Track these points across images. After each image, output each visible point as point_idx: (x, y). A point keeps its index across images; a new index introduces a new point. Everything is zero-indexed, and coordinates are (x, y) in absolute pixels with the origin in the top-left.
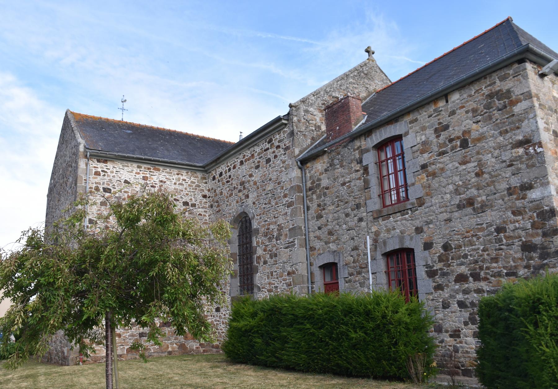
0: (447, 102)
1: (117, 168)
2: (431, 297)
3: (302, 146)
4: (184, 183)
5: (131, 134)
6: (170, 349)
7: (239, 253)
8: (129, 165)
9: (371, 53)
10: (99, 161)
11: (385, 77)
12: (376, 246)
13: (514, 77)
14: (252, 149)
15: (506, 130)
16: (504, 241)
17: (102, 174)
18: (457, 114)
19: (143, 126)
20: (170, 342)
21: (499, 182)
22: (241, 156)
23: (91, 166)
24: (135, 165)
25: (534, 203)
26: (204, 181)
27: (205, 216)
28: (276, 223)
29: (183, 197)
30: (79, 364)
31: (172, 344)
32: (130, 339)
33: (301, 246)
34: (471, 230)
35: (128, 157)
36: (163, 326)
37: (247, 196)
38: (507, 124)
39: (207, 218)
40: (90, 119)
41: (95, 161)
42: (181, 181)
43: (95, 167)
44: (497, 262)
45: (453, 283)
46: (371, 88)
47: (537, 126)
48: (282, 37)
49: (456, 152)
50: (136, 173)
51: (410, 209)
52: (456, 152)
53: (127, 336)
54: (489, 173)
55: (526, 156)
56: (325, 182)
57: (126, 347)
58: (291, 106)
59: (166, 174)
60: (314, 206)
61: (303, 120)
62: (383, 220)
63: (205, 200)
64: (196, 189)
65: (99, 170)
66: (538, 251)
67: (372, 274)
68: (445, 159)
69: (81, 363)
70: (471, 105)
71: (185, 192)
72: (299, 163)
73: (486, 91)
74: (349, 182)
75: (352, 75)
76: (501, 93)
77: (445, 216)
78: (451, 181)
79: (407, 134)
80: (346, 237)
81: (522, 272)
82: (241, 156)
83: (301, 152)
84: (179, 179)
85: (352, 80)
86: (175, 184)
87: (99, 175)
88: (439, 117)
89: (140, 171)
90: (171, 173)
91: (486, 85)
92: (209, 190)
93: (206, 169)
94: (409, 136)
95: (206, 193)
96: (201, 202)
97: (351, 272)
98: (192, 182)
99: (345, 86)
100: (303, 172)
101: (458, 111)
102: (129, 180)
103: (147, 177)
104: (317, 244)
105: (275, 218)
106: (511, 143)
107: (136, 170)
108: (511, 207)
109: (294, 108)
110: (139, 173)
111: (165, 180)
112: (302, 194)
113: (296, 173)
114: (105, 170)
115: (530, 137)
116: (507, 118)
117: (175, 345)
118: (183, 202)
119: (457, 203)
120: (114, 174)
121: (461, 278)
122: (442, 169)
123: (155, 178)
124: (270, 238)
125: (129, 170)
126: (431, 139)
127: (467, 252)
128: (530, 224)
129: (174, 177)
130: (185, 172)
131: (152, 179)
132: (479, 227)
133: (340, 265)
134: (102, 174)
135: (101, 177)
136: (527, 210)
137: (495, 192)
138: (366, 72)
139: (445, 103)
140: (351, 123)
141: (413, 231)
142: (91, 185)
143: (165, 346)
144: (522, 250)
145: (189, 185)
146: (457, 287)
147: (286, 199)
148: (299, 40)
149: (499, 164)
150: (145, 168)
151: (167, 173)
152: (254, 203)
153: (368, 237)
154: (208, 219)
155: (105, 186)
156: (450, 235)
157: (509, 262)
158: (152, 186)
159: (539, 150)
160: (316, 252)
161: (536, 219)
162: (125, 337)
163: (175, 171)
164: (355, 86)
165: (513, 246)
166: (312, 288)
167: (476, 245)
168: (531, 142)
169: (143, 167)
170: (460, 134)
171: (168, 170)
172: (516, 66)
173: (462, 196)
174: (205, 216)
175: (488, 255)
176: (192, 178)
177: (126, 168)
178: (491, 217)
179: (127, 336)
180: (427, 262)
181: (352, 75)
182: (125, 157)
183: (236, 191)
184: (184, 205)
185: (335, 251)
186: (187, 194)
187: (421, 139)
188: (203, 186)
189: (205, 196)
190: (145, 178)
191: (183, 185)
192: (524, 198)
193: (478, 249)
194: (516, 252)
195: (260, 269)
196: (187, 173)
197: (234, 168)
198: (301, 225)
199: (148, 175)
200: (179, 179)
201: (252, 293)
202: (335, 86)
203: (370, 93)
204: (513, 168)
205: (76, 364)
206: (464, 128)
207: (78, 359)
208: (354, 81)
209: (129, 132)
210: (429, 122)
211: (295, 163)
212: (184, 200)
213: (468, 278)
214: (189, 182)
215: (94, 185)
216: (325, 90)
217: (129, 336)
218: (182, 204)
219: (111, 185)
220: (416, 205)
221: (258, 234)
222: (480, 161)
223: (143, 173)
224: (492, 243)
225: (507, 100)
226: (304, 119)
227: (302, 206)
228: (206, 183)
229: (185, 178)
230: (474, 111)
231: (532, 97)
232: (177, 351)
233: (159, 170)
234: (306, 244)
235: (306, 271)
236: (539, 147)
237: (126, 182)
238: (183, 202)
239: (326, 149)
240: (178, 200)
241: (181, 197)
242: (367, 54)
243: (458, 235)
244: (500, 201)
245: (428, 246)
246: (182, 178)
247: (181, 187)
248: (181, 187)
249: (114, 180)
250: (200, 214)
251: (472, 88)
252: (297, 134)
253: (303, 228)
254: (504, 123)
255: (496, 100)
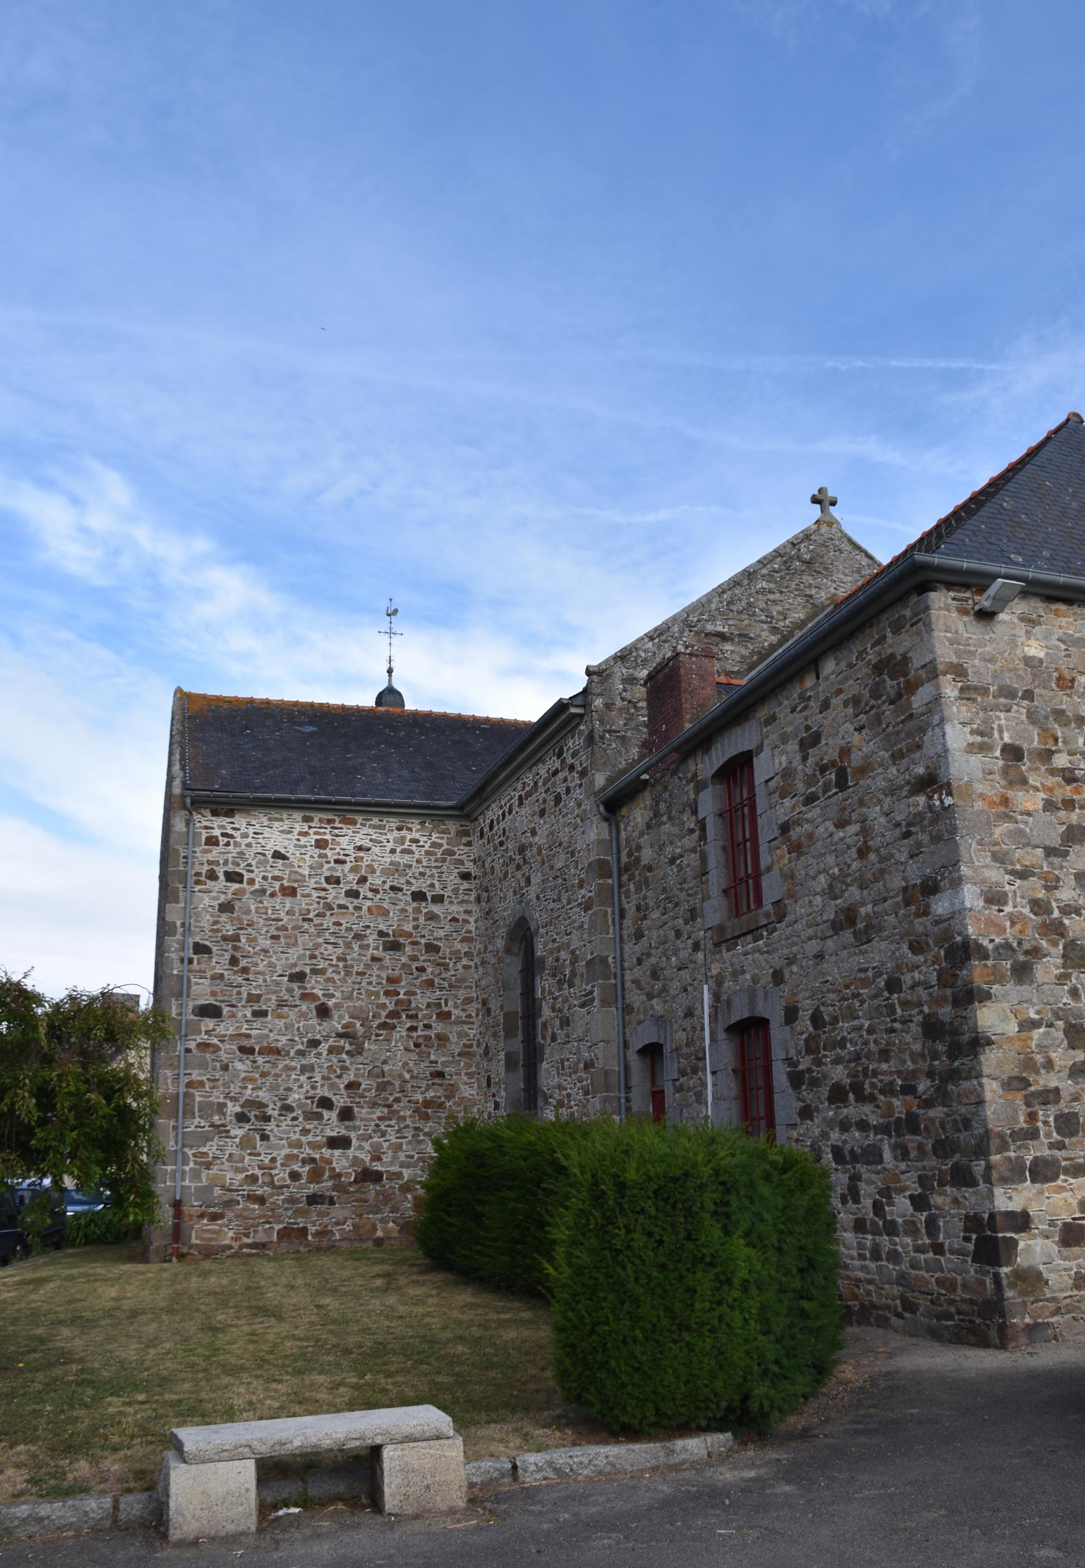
0: (818, 678)
1: (257, 826)
2: (795, 1135)
3: (614, 766)
4: (414, 847)
5: (312, 735)
6: (379, 1234)
7: (523, 1012)
8: (285, 816)
9: (827, 503)
10: (215, 813)
11: (865, 561)
12: (716, 1008)
13: (912, 625)
14: (534, 770)
15: (901, 750)
16: (899, 1011)
17: (223, 841)
18: (832, 706)
19: (350, 708)
20: (379, 1216)
21: (890, 873)
22: (519, 786)
23: (198, 825)
24: (298, 816)
25: (941, 926)
26: (465, 840)
27: (466, 921)
28: (568, 945)
29: (412, 880)
30: (170, 1261)
31: (384, 1221)
32: (286, 1209)
33: (605, 1003)
34: (852, 983)
35: (277, 800)
36: (364, 1181)
37: (528, 881)
38: (903, 735)
39: (472, 927)
40: (226, 706)
41: (207, 813)
42: (408, 843)
43: (206, 828)
44: (887, 1061)
45: (826, 1104)
46: (822, 596)
47: (944, 745)
48: (894, 363)
49: (829, 797)
50: (300, 834)
51: (765, 926)
52: (829, 797)
53: (280, 1203)
54: (877, 850)
55: (929, 815)
56: (647, 855)
57: (277, 1227)
58: (589, 672)
59: (371, 831)
60: (630, 908)
61: (619, 703)
62: (729, 950)
63: (465, 885)
64: (444, 860)
65: (217, 832)
66: (947, 1038)
67: (713, 1073)
68: (814, 813)
69: (174, 1259)
70: (852, 688)
71: (417, 870)
72: (602, 808)
73: (872, 657)
74: (681, 856)
75: (764, 571)
76: (893, 661)
77: (813, 947)
78: (822, 866)
79: (760, 748)
80: (675, 985)
81: (923, 1085)
82: (519, 786)
83: (610, 780)
84: (402, 841)
85: (764, 584)
86: (393, 851)
87: (217, 844)
88: (805, 713)
89: (310, 827)
90: (382, 827)
91: (873, 641)
92: (474, 861)
93: (466, 811)
94: (762, 755)
95: (470, 867)
96: (456, 891)
97: (683, 1066)
98: (434, 845)
99: (744, 603)
100: (614, 830)
101: (833, 701)
102: (283, 851)
103: (326, 841)
104: (636, 997)
105: (567, 935)
106: (908, 782)
107: (298, 827)
108: (907, 934)
109: (595, 678)
110: (306, 834)
111: (369, 844)
112: (610, 881)
113: (596, 831)
114: (230, 831)
115: (935, 769)
116: (903, 722)
117: (391, 1224)
118: (413, 893)
119: (832, 917)
120: (250, 840)
121: (837, 1095)
122: (810, 836)
123: (344, 842)
124: (560, 980)
125: (285, 827)
126: (794, 764)
127: (846, 1034)
128: (935, 974)
129: (389, 836)
130: (417, 822)
131: (339, 844)
132: (862, 975)
133: (667, 1050)
134: (223, 841)
135: (221, 848)
136: (931, 943)
137: (885, 895)
138: (807, 557)
139: (814, 681)
140: (682, 717)
141: (770, 979)
142: (197, 868)
143: (369, 1227)
144: (924, 1035)
145: (427, 853)
146: (831, 1113)
147: (583, 892)
148: (943, 364)
149: (891, 830)
150: (321, 820)
151: (374, 827)
152: (538, 898)
153: (706, 987)
154: (473, 929)
155: (230, 868)
156: (823, 992)
157: (905, 1062)
158: (337, 861)
159: (949, 801)
160: (633, 1018)
161: (944, 964)
162: (274, 1203)
163: (394, 822)
164: (771, 597)
165: (911, 1025)
166: (628, 1100)
167: (858, 1018)
168: (936, 782)
169: (316, 819)
170: (835, 756)
171: (375, 821)
172: (915, 598)
173: (839, 901)
174: (466, 921)
175: (876, 1042)
176: (434, 835)
177: (276, 824)
178: (881, 953)
179: (280, 1203)
180: (787, 1053)
181: (764, 571)
182: (269, 800)
183: (512, 868)
184: (414, 900)
185: (661, 1017)
186: (422, 874)
187: (780, 764)
188: (461, 851)
189: (466, 876)
190: (321, 844)
191: (413, 853)
192: (926, 913)
193: (861, 1028)
194: (912, 1038)
195: (547, 1051)
196: (422, 823)
197: (510, 812)
198: (606, 954)
199: (328, 837)
200: (402, 841)
201: (536, 1108)
202: (713, 606)
203: (817, 609)
204: (910, 841)
205: (165, 1261)
206: (842, 742)
207: (170, 1251)
208: (772, 586)
209: (310, 729)
210: (791, 723)
211: (595, 809)
212: (413, 889)
213: (846, 1093)
214: (428, 844)
215: (206, 867)
216: (686, 620)
217: (284, 1201)
218: (409, 899)
219: (243, 865)
220: (773, 918)
221: (544, 969)
222: (864, 821)
223: (315, 833)
224: (881, 1014)
225: (902, 679)
226: (623, 699)
227: (609, 910)
228: (469, 844)
229: (416, 835)
230: (856, 701)
231: (936, 676)
232: (395, 1238)
233: (353, 822)
234: (616, 997)
235: (616, 1062)
236: (947, 795)
237: (277, 855)
238: (413, 893)
239: (645, 777)
240: (400, 890)
241: (408, 882)
242: (818, 506)
243: (833, 992)
244: (891, 919)
245: (791, 1015)
246: (409, 837)
247: (406, 859)
248: (406, 859)
249: (250, 853)
250: (454, 920)
251: (853, 647)
252: (602, 738)
253: (610, 960)
254: (898, 733)
255: (886, 677)
